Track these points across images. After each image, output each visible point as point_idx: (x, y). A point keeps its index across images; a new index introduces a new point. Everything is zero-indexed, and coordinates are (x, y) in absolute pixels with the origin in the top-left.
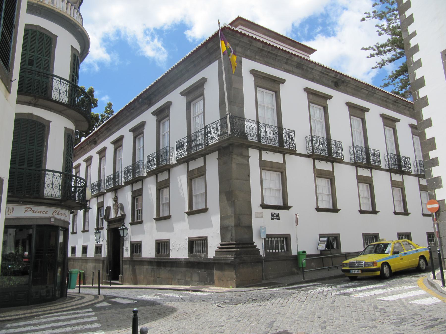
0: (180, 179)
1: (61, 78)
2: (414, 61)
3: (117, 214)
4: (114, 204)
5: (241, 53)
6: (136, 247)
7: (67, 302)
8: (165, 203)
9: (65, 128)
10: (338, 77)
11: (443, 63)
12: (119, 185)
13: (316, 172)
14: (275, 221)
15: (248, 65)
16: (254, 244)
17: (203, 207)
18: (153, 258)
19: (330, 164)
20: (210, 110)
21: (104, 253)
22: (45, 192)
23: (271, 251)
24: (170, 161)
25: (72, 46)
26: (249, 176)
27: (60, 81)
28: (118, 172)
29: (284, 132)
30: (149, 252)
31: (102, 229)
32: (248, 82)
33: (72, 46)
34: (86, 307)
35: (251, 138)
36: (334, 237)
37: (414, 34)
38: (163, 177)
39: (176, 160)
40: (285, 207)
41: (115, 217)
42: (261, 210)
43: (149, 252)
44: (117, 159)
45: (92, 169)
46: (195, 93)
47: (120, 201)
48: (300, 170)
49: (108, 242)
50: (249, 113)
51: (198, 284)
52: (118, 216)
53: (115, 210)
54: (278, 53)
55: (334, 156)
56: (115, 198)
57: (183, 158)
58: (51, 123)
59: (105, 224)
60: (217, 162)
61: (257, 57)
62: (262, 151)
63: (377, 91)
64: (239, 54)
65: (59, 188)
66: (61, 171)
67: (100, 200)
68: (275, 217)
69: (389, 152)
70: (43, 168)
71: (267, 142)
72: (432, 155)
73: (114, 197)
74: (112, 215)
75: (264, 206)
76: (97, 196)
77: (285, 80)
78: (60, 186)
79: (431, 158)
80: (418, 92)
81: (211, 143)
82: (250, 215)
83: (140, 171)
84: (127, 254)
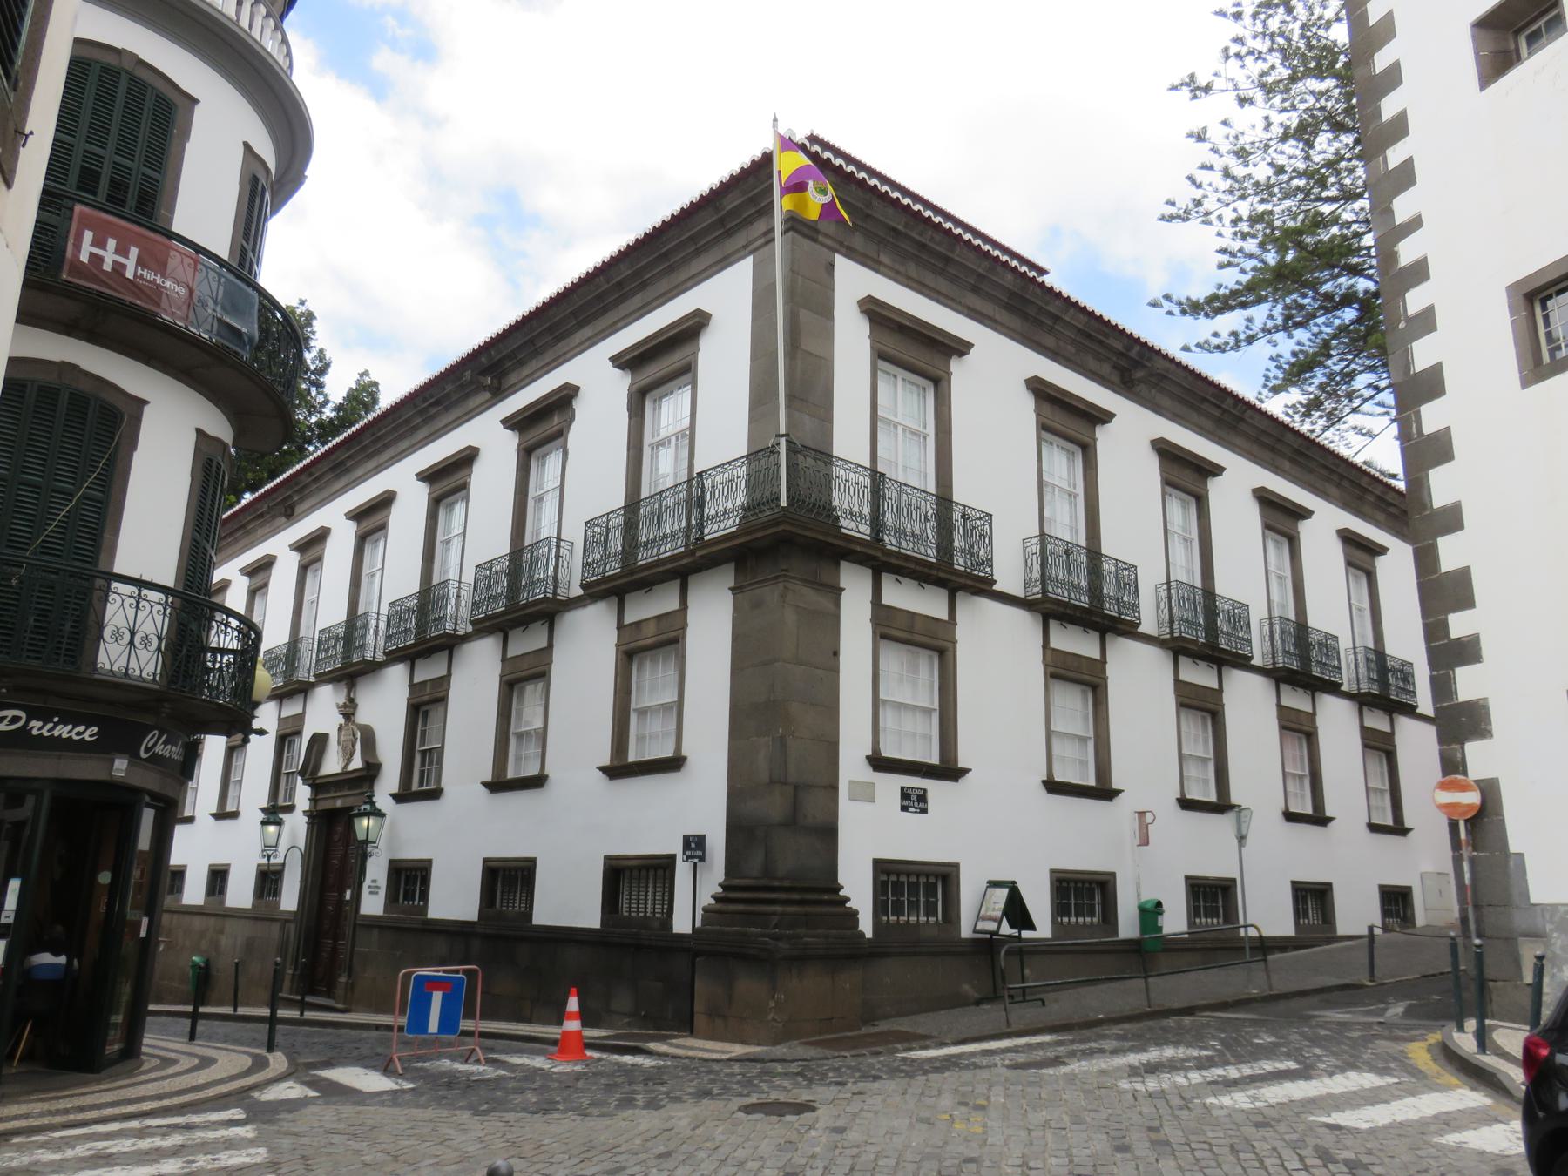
0: (586, 648)
1: (199, 249)
2: (1410, 313)
3: (349, 761)
4: (340, 728)
5: (835, 240)
6: (411, 878)
7: (144, 1077)
8: (528, 733)
9: (199, 431)
10: (1133, 354)
11: (1513, 322)
12: (364, 661)
13: (1049, 659)
14: (912, 818)
15: (853, 282)
16: (842, 893)
17: (667, 752)
19: (1094, 637)
20: (716, 418)
21: (289, 899)
22: (103, 660)
23: (893, 918)
24: (555, 587)
25: (247, 145)
26: (836, 654)
27: (196, 262)
28: (366, 614)
29: (957, 515)
30: (454, 898)
31: (290, 809)
32: (851, 341)
33: (247, 145)
34: (221, 1102)
35: (853, 525)
36: (936, 877)
37: (1415, 223)
38: (526, 642)
39: (582, 586)
40: (949, 771)
41: (338, 769)
42: (867, 774)
43: (454, 898)
44: (366, 570)
45: (285, 592)
46: (662, 363)
47: (362, 717)
48: (999, 652)
49: (306, 857)
50: (849, 439)
51: (629, 1025)
52: (351, 767)
53: (344, 749)
54: (953, 251)
55: (1110, 609)
56: (345, 706)
57: (605, 580)
58: (147, 409)
59: (302, 795)
60: (728, 599)
61: (884, 259)
62: (884, 575)
63: (1249, 412)
64: (828, 242)
65: (159, 649)
66: (170, 583)
67: (292, 709)
68: (914, 801)
69: (1276, 613)
70: (102, 567)
71: (904, 544)
72: (1459, 625)
73: (342, 700)
74: (332, 764)
75: (879, 763)
76: (280, 696)
77: (969, 346)
78: (160, 639)
79: (1454, 634)
80: (1418, 414)
81: (712, 532)
82: (833, 788)
83: (444, 617)
84: (372, 904)
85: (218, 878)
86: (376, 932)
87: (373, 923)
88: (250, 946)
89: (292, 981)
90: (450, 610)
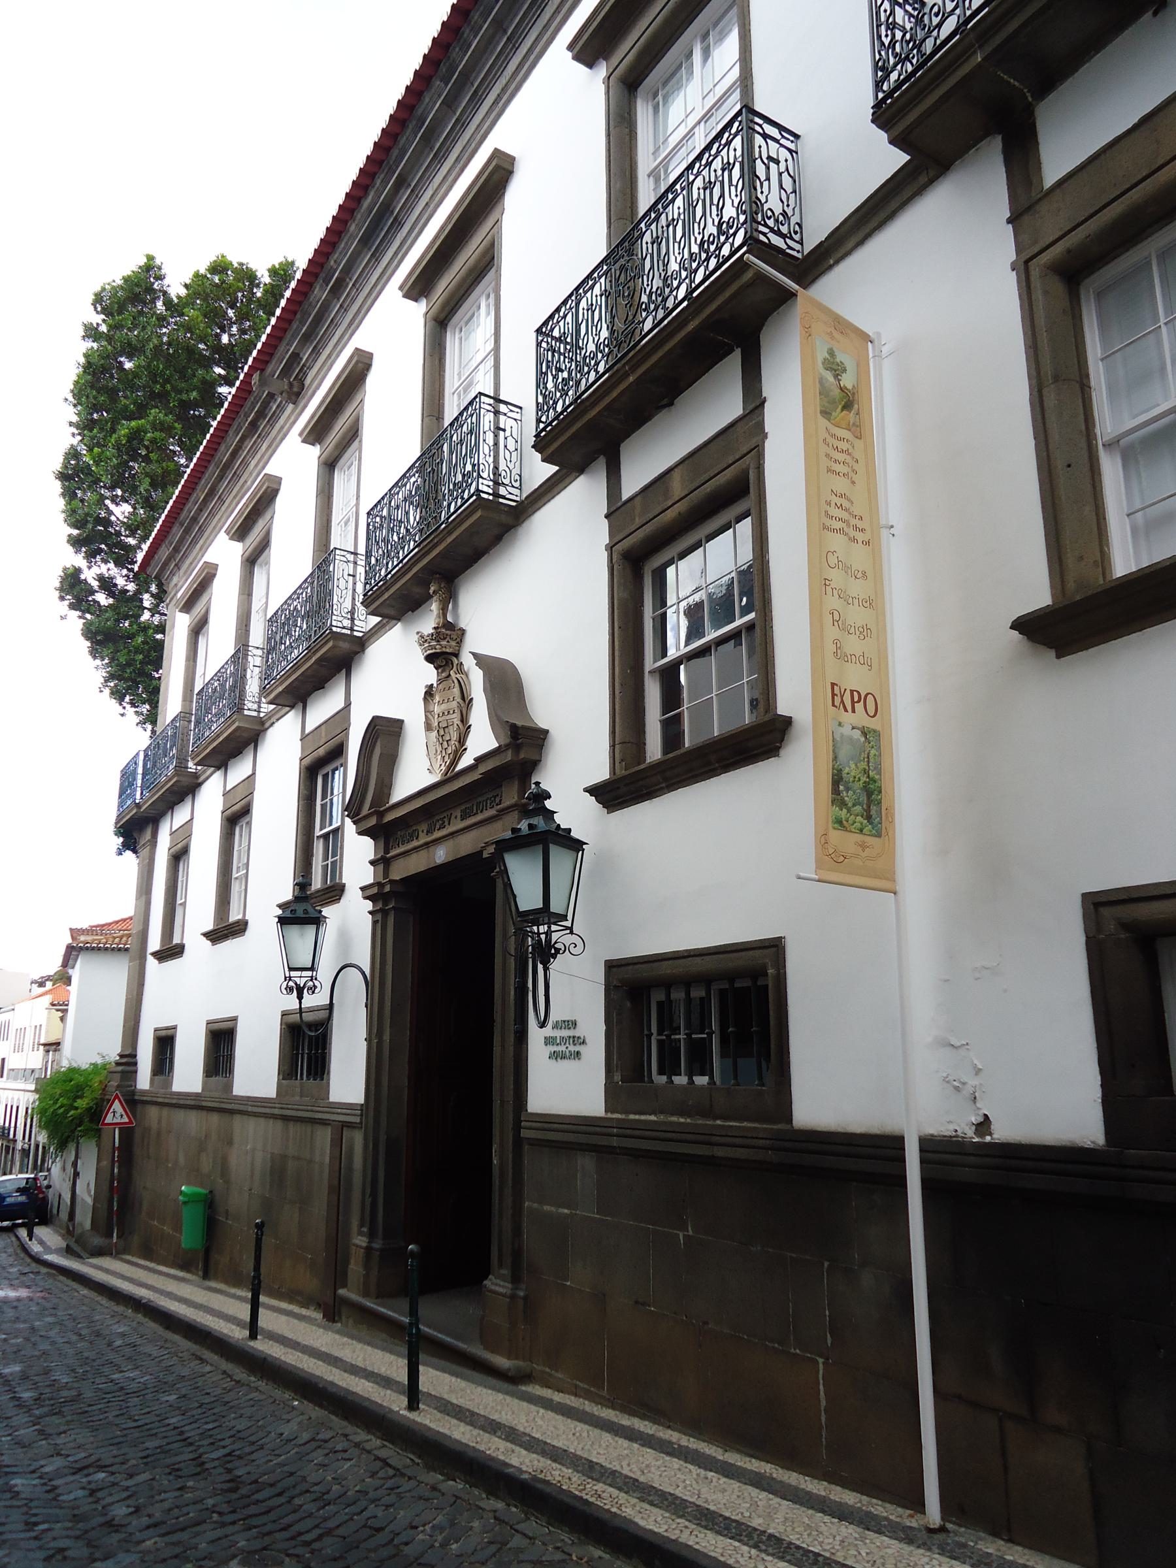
4: (429, 693)
18: (197, 1095)
21: (347, 1080)
31: (334, 892)
59: (358, 857)
85: (221, 1041)
86: (586, 1163)
87: (569, 1135)
88: (278, 1171)
89: (367, 1265)
90: (485, 457)
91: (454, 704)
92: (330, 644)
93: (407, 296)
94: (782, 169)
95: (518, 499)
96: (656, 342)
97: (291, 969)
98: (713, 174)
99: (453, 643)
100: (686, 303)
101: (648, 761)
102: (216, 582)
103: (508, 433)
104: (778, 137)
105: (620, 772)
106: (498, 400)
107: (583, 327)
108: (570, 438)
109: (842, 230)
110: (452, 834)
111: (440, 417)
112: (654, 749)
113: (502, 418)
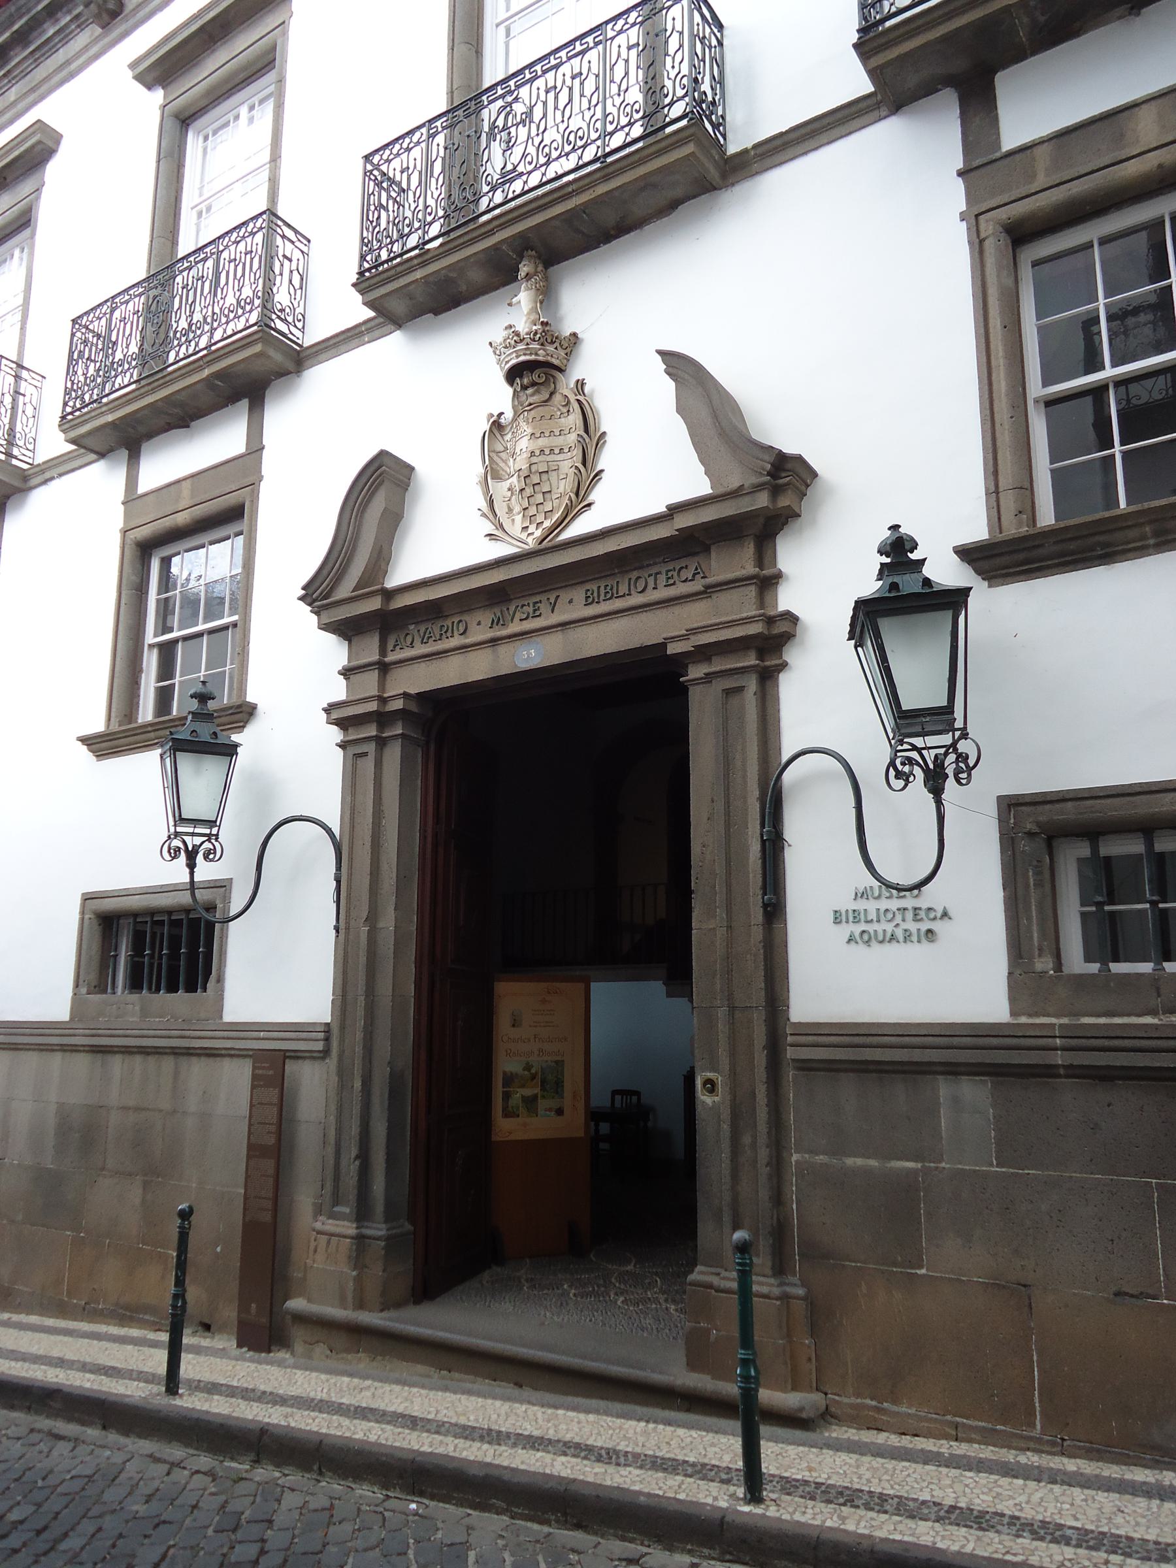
86: (975, 1093)
91: (573, 437)
92: (258, 348)
93: (139, 78)
94: (294, 267)
95: (30, 461)
96: (902, 30)
97: (181, 820)
98: (534, 92)
99: (562, 353)
100: (684, 122)
101: (140, 721)
102: (53, 169)
103: (27, 399)
104: (294, 239)
105: (115, 727)
106: (20, 366)
107: (223, 275)
108: (945, 39)
109: (786, 138)
110: (564, 625)
111: (174, 242)
112: (147, 712)
113: (23, 383)
